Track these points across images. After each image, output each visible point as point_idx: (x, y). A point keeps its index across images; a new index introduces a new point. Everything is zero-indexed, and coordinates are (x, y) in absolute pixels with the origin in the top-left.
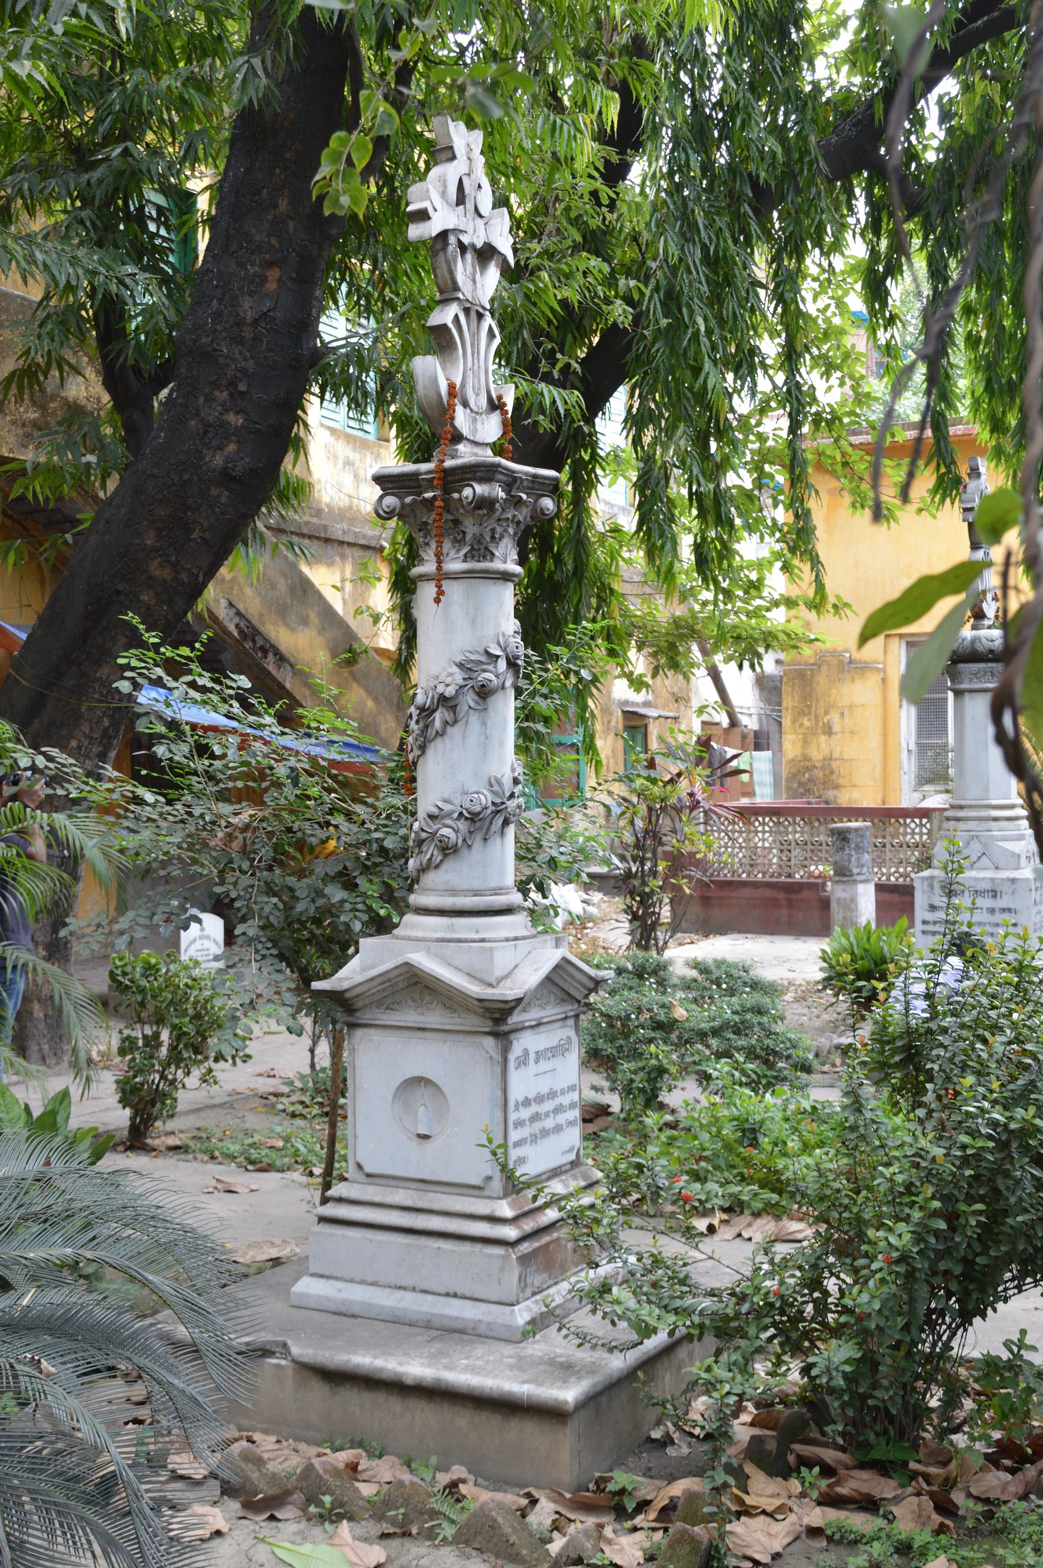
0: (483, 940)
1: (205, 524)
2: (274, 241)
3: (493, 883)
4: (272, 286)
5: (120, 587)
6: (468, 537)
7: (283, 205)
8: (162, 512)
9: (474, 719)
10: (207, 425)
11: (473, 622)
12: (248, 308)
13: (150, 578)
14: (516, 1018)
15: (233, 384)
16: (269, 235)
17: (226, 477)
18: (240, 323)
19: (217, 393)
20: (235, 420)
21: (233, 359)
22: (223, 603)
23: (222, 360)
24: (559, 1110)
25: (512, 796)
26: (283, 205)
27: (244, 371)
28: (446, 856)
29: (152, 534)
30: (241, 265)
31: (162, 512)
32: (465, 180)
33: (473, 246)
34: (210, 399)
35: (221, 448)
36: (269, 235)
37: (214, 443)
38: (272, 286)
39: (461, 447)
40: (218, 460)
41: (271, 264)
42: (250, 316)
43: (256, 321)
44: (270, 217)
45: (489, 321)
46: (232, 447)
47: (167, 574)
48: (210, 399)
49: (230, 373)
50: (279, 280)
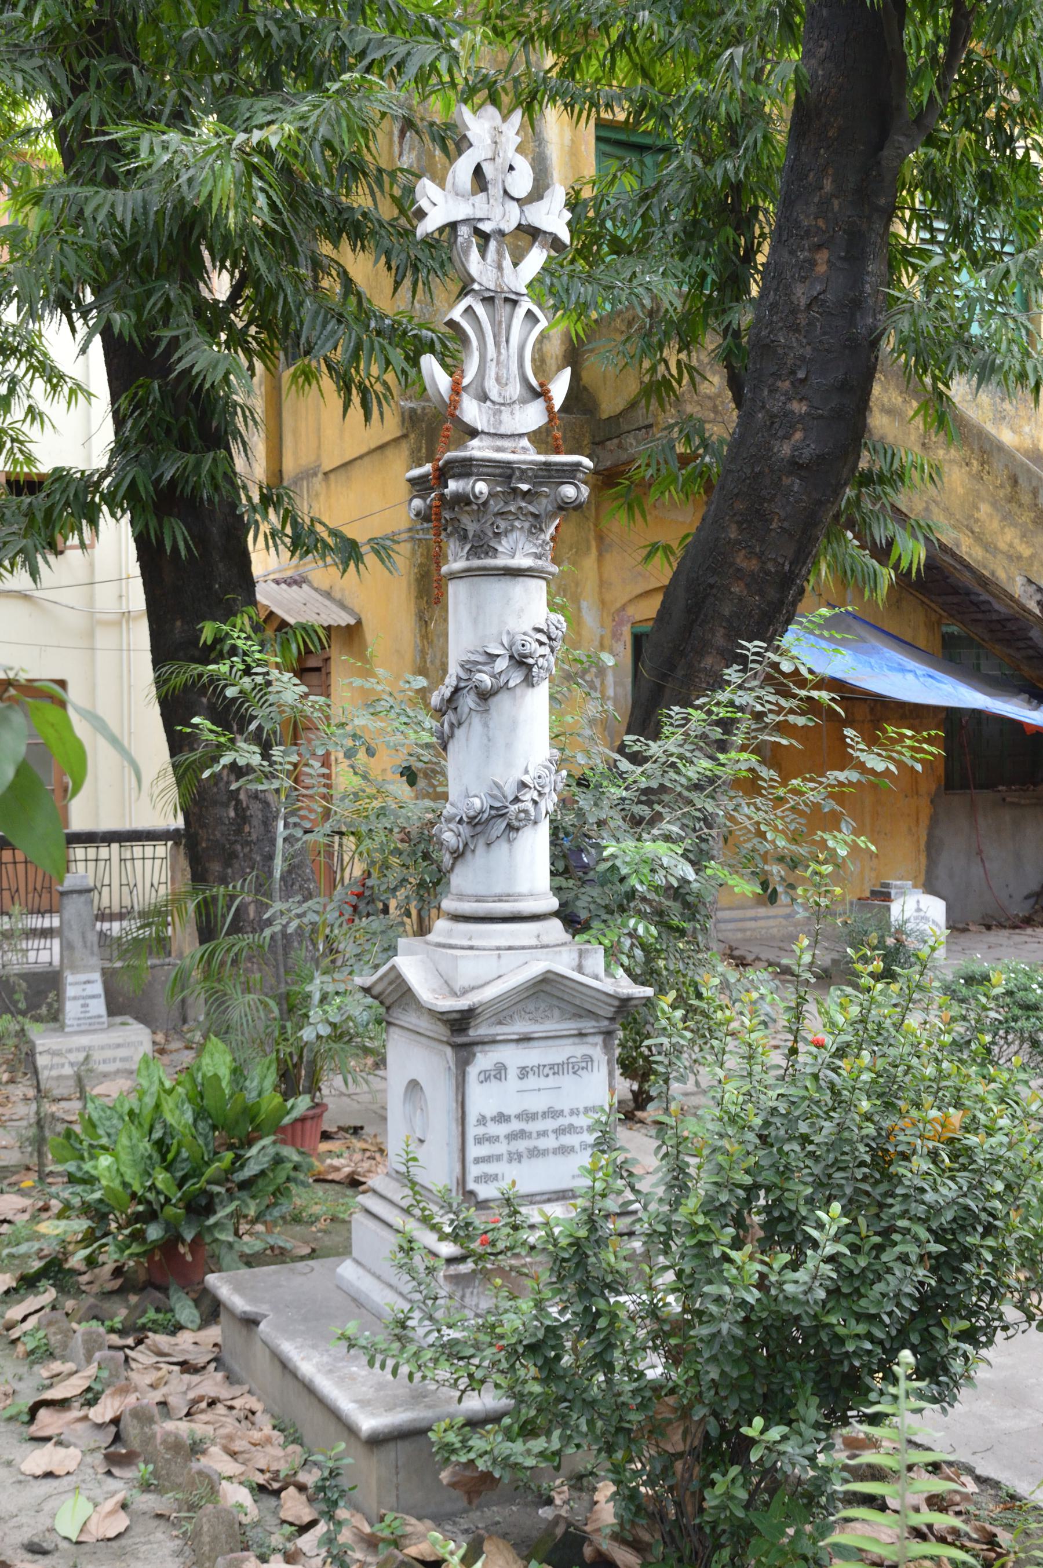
0: (471, 948)
1: (782, 514)
2: (821, 223)
3: (498, 890)
4: (822, 268)
5: (712, 581)
6: (470, 535)
7: (828, 185)
8: (740, 506)
9: (476, 721)
10: (773, 416)
11: (475, 621)
12: (801, 294)
13: (739, 570)
14: (479, 1031)
15: (793, 373)
16: (816, 218)
17: (795, 466)
18: (794, 311)
19: (779, 384)
20: (799, 408)
21: (791, 348)
22: (1020, 580)
23: (780, 351)
24: (571, 1129)
25: (517, 800)
26: (828, 185)
27: (802, 358)
28: (456, 859)
29: (734, 527)
30: (792, 253)
31: (740, 506)
32: (487, 168)
33: (501, 233)
34: (773, 390)
35: (787, 437)
36: (816, 218)
37: (780, 433)
38: (822, 268)
39: (475, 443)
40: (786, 450)
41: (819, 247)
42: (803, 302)
43: (809, 306)
44: (816, 200)
45: (526, 304)
46: (798, 435)
47: (753, 565)
48: (773, 390)
49: (790, 362)
50: (829, 261)
